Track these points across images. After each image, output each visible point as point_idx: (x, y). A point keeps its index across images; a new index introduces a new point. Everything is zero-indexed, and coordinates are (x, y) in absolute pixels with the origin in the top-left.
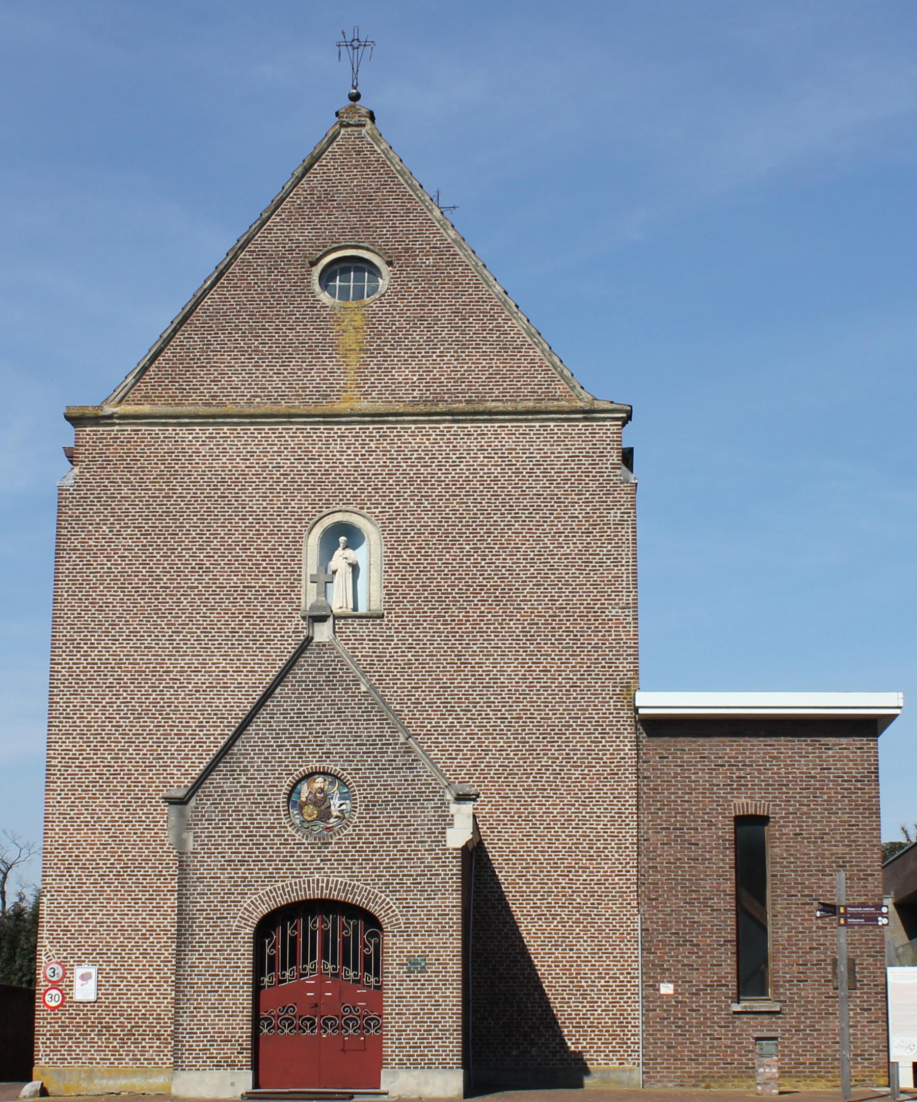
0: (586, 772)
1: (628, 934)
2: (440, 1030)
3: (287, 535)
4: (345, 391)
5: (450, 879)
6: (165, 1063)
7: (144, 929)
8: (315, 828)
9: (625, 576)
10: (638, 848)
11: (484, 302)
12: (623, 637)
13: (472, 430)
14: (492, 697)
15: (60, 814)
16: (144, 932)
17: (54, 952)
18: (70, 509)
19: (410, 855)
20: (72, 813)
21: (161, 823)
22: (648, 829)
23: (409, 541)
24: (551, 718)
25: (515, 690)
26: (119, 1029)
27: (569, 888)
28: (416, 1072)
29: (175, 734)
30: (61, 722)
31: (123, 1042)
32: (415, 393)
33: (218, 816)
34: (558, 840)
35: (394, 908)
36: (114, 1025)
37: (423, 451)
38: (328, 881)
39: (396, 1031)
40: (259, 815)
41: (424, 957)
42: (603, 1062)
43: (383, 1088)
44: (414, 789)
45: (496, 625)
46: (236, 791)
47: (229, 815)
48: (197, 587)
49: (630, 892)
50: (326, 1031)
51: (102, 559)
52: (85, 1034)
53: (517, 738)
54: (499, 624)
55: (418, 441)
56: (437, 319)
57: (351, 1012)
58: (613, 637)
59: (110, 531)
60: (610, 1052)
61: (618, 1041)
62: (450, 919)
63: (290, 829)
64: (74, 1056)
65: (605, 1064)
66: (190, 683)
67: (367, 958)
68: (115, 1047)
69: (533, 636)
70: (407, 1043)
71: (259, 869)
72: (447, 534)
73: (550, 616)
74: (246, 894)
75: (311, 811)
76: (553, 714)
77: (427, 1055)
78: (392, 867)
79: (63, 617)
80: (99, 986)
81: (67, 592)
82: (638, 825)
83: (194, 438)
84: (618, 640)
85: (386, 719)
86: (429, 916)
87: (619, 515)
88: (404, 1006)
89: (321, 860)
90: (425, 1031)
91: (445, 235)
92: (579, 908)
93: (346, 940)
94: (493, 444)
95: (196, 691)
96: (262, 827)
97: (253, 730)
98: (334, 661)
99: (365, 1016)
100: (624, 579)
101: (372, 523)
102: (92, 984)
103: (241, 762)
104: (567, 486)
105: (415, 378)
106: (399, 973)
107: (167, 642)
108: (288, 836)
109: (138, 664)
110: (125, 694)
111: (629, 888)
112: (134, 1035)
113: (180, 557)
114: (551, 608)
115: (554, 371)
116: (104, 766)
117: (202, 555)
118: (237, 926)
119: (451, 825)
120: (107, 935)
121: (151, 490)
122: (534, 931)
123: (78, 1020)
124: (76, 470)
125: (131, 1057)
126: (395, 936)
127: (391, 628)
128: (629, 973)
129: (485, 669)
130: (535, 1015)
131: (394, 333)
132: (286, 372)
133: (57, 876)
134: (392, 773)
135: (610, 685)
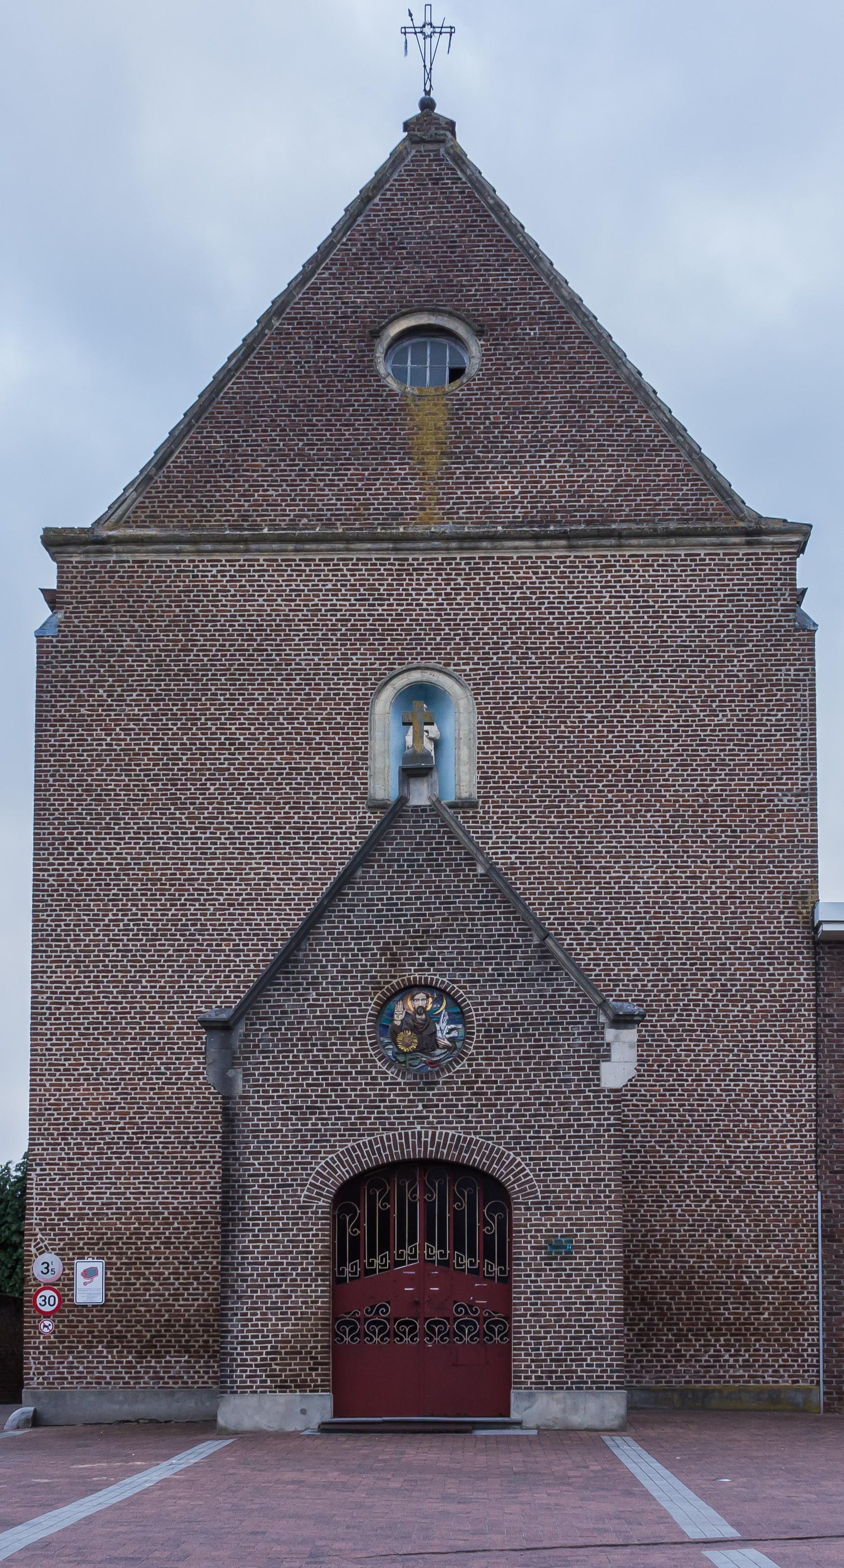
0: (748, 1008)
1: (803, 1216)
2: (593, 1337)
3: (346, 700)
4: (422, 509)
5: (605, 1131)
6: (197, 1383)
7: (166, 1212)
8: (416, 1062)
9: (800, 753)
10: (817, 1106)
11: (609, 387)
12: (797, 833)
13: (595, 560)
14: (623, 911)
15: (50, 1065)
16: (166, 1215)
17: (46, 1242)
18: (53, 667)
19: (549, 1098)
20: (67, 1063)
21: (187, 1075)
22: (831, 1082)
23: (510, 708)
24: (701, 939)
25: (654, 903)
26: (135, 1340)
27: (726, 1157)
28: (561, 1394)
29: (203, 961)
30: (50, 946)
31: (140, 1356)
32: (517, 511)
33: (277, 1046)
34: (712, 1096)
35: (528, 1171)
36: (129, 1335)
37: (528, 588)
38: (434, 1134)
39: (532, 1338)
40: (335, 1044)
41: (570, 1236)
42: (771, 1379)
43: (515, 1416)
44: (555, 1008)
45: (628, 818)
46: (302, 1011)
47: (293, 1045)
48: (229, 769)
49: (807, 1163)
50: (431, 1339)
51: (99, 733)
52: (89, 1347)
53: (657, 965)
54: (632, 816)
55: (522, 575)
56: (545, 412)
57: (467, 1313)
58: (784, 833)
59: (108, 696)
60: (780, 1366)
61: (791, 1352)
62: (606, 1186)
63: (379, 1064)
64: (76, 1375)
65: (774, 1382)
66: (222, 895)
67: (488, 1241)
68: (131, 1362)
69: (678, 832)
70: (546, 1355)
71: (336, 1119)
72: (561, 698)
73: (699, 806)
74: (320, 1152)
75: (408, 1041)
76: (704, 933)
77: (576, 1371)
78: (525, 1116)
79: (48, 810)
80: (108, 1285)
81: (51, 776)
82: (817, 1076)
83: (218, 571)
84: (791, 838)
85: (514, 912)
86: (576, 1182)
87: (792, 673)
88: (542, 1304)
89: (424, 1106)
90: (572, 1338)
91: (556, 295)
92: (739, 1182)
93: (458, 1216)
94: (623, 579)
95: (230, 905)
96: (341, 1062)
97: (325, 928)
98: (438, 832)
99: (486, 1319)
100: (800, 757)
101: (461, 684)
102: (98, 1282)
103: (309, 972)
104: (722, 635)
105: (517, 492)
106: (535, 1259)
107: (190, 841)
108: (377, 1072)
109: (152, 869)
110: (134, 909)
111: (805, 1157)
112: (156, 1347)
113: (204, 730)
114: (702, 796)
115: (705, 481)
116: (108, 1003)
117: (233, 727)
118: (306, 1196)
119: (607, 1058)
120: (117, 1219)
121: (162, 641)
122: (679, 1211)
123: (80, 1329)
124: (60, 615)
125: (151, 1374)
126: (529, 1209)
127: (488, 822)
128: (806, 1267)
129: (613, 875)
130: (681, 1320)
131: (487, 431)
132: (341, 484)
133: (48, 1144)
134: (523, 986)
135: (781, 895)
